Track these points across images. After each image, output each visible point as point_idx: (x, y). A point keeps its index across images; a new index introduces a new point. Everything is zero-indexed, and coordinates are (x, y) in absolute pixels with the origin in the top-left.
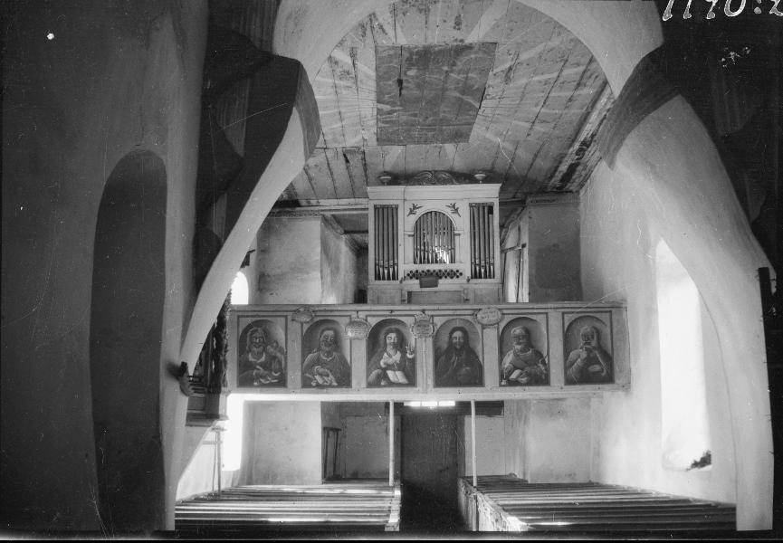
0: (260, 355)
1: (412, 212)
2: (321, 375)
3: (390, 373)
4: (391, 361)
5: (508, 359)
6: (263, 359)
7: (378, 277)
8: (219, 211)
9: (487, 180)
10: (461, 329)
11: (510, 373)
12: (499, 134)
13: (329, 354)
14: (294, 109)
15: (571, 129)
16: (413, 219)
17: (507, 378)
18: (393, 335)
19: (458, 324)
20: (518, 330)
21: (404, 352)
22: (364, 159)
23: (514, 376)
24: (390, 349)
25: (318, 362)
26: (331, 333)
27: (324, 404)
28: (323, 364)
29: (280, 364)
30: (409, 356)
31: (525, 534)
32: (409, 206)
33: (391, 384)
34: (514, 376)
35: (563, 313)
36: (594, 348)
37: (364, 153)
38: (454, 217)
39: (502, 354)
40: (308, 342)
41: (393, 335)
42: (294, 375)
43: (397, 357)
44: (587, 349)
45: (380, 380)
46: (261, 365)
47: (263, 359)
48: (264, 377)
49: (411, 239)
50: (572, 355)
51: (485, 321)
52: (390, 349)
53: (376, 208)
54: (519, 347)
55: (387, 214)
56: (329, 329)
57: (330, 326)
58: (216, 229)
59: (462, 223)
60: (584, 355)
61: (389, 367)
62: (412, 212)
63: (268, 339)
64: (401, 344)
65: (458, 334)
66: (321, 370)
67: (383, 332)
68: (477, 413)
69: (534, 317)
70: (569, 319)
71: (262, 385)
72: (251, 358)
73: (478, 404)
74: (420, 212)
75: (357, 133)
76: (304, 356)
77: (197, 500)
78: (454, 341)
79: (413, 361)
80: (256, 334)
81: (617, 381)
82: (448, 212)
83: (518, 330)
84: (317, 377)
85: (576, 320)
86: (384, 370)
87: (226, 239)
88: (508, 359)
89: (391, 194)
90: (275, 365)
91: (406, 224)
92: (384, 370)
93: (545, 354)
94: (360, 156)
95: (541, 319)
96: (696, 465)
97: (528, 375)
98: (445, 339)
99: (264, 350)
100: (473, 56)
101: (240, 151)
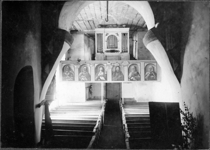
1: (106, 35)
2: (83, 78)
3: (101, 77)
4: (101, 74)
5: (130, 74)
6: (69, 74)
7: (98, 52)
8: (47, 68)
9: (126, 27)
11: (131, 78)
12: (128, 17)
13: (85, 73)
16: (107, 37)
17: (130, 79)
20: (133, 67)
22: (93, 22)
23: (132, 78)
24: (100, 71)
25: (82, 75)
29: (73, 75)
32: (106, 33)
35: (144, 63)
36: (152, 72)
37: (93, 21)
38: (117, 37)
40: (80, 70)
42: (77, 78)
43: (102, 73)
44: (150, 72)
46: (68, 75)
47: (69, 74)
48: (69, 78)
50: (147, 73)
51: (124, 65)
52: (100, 71)
53: (97, 34)
54: (133, 71)
55: (100, 35)
56: (85, 66)
57: (85, 66)
58: (47, 72)
59: (120, 38)
60: (150, 73)
63: (70, 69)
64: (103, 70)
66: (83, 77)
67: (99, 67)
69: (137, 64)
70: (146, 64)
74: (108, 35)
75: (91, 17)
76: (79, 74)
78: (117, 70)
80: (66, 68)
81: (158, 80)
82: (116, 35)
83: (133, 67)
84: (82, 78)
85: (148, 65)
86: (99, 77)
88: (130, 74)
89: (99, 31)
90: (72, 75)
91: (105, 38)
93: (140, 73)
94: (92, 21)
95: (139, 64)
97: (135, 78)
99: (69, 72)
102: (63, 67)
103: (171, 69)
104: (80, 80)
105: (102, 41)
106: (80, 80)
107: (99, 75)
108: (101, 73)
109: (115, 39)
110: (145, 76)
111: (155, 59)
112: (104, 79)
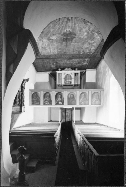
0: (35, 99)
3: (59, 102)
6: (36, 99)
8: (12, 67)
10: (73, 94)
11: (81, 102)
13: (48, 99)
14: (29, 43)
15: (98, 61)
16: (65, 75)
18: (60, 95)
19: (72, 93)
20: (83, 95)
21: (62, 99)
24: (59, 98)
26: (48, 95)
27: (48, 108)
28: (47, 101)
30: (63, 99)
31: (78, 147)
33: (59, 104)
34: (82, 103)
39: (80, 99)
41: (60, 95)
43: (61, 99)
45: (57, 104)
46: (36, 100)
47: (36, 99)
49: (64, 79)
50: (93, 100)
58: (11, 71)
59: (73, 76)
61: (59, 101)
62: (64, 74)
65: (72, 95)
66: (47, 102)
67: (58, 94)
68: (75, 109)
71: (36, 104)
72: (34, 99)
73: (75, 108)
77: (23, 126)
79: (63, 100)
84: (46, 103)
86: (58, 102)
87: (14, 72)
92: (58, 102)
96: (27, 80)
98: (70, 96)
100: (76, 39)
101: (16, 53)
102: (32, 94)
103: (104, 83)
104: (44, 104)
105: (61, 79)
106: (44, 104)
107: (58, 100)
108: (59, 99)
109: (70, 76)
110: (92, 101)
111: (89, 141)
112: (61, 103)
